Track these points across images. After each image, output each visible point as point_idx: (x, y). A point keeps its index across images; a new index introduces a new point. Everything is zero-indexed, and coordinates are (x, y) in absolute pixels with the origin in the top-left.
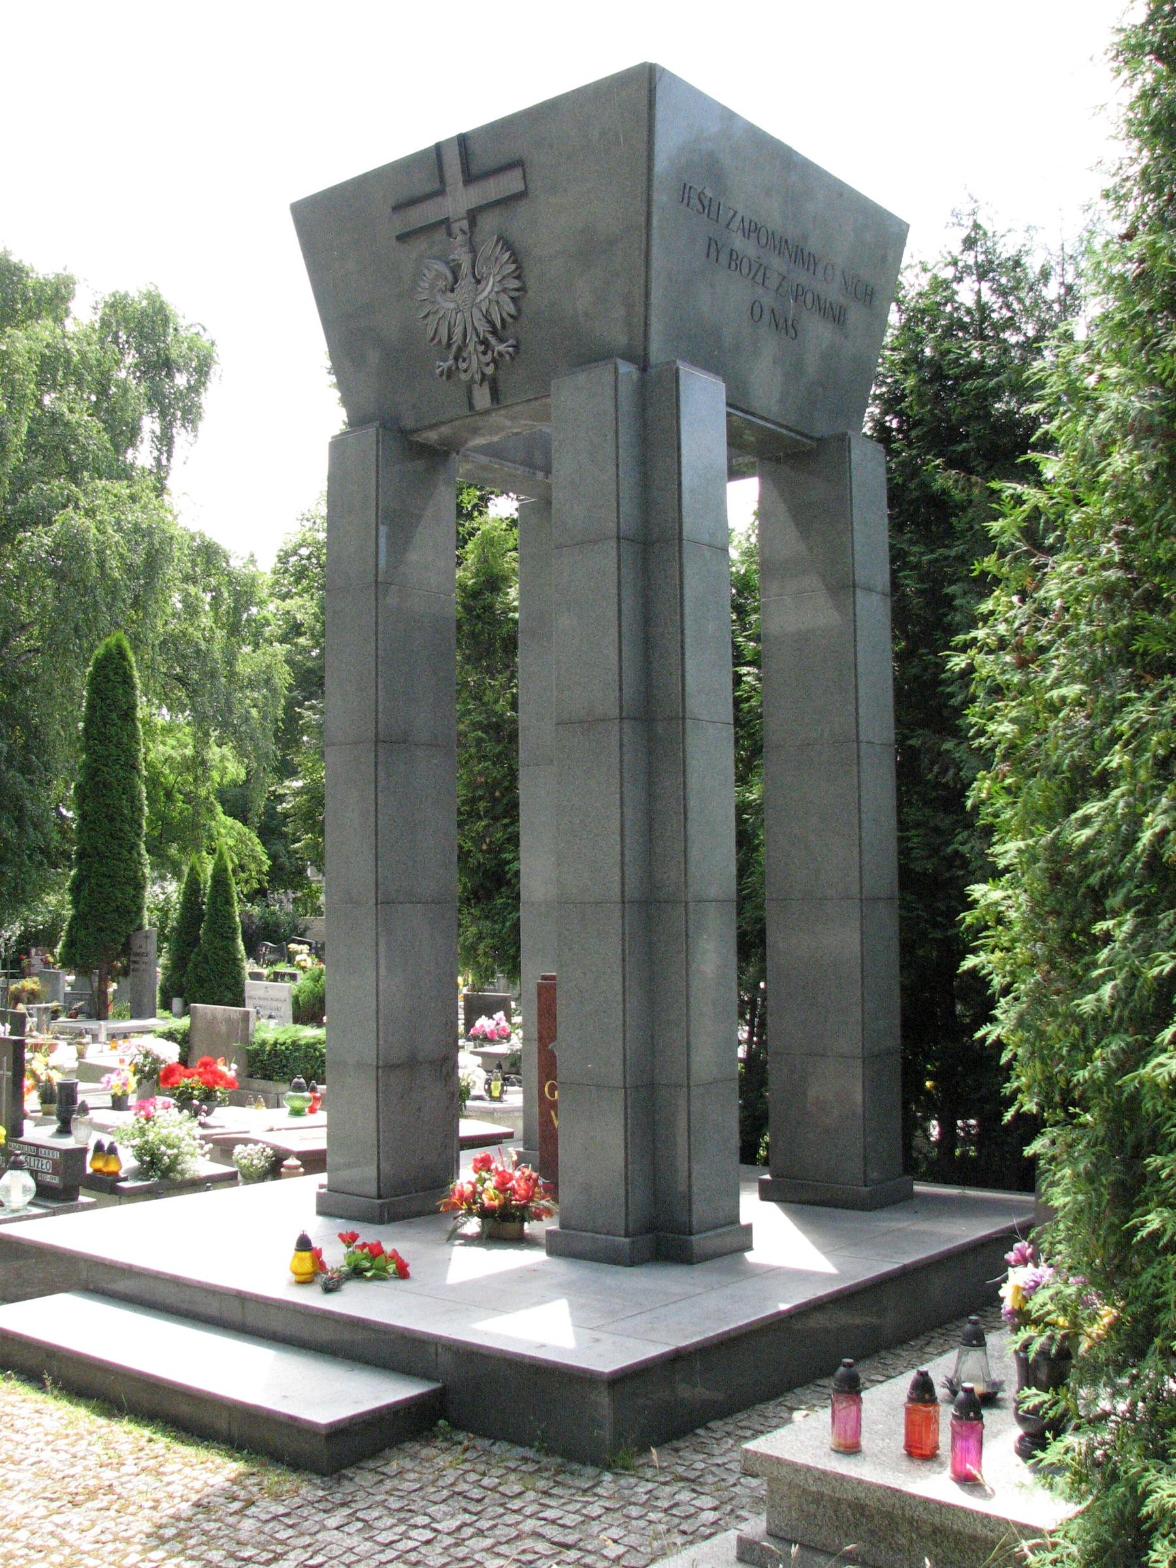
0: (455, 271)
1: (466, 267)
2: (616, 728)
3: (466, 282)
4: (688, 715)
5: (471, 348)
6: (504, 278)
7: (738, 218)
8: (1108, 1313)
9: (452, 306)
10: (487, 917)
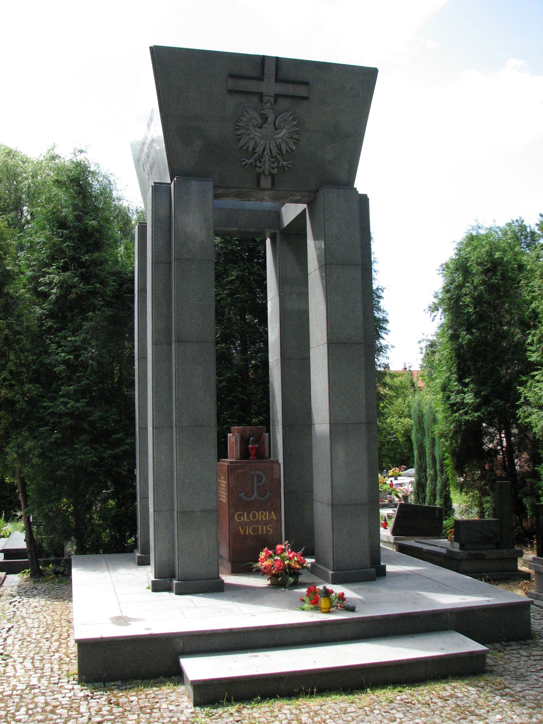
0: (265, 119)
8: (110, 501)
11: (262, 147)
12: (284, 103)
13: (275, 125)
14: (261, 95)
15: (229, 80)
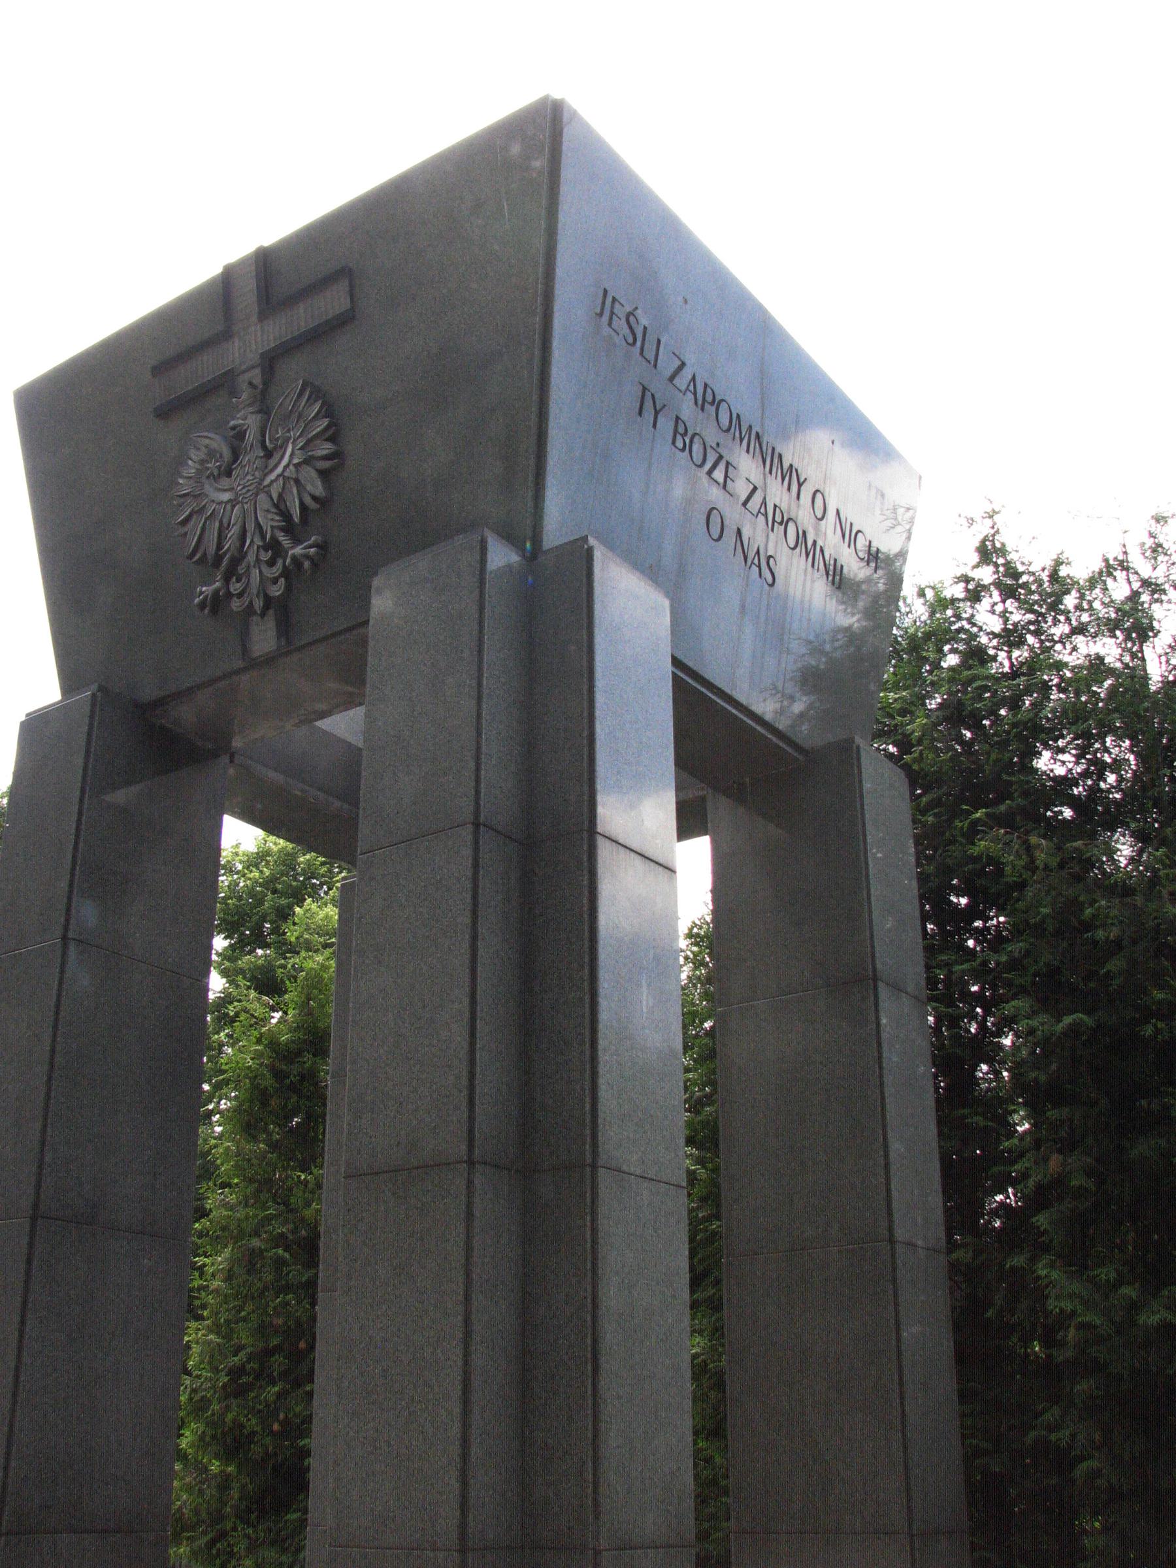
1: (251, 436)
2: (461, 1182)
3: (251, 458)
4: (603, 1159)
5: (251, 558)
6: (309, 442)
7: (687, 374)
9: (226, 496)
10: (273, 1543)
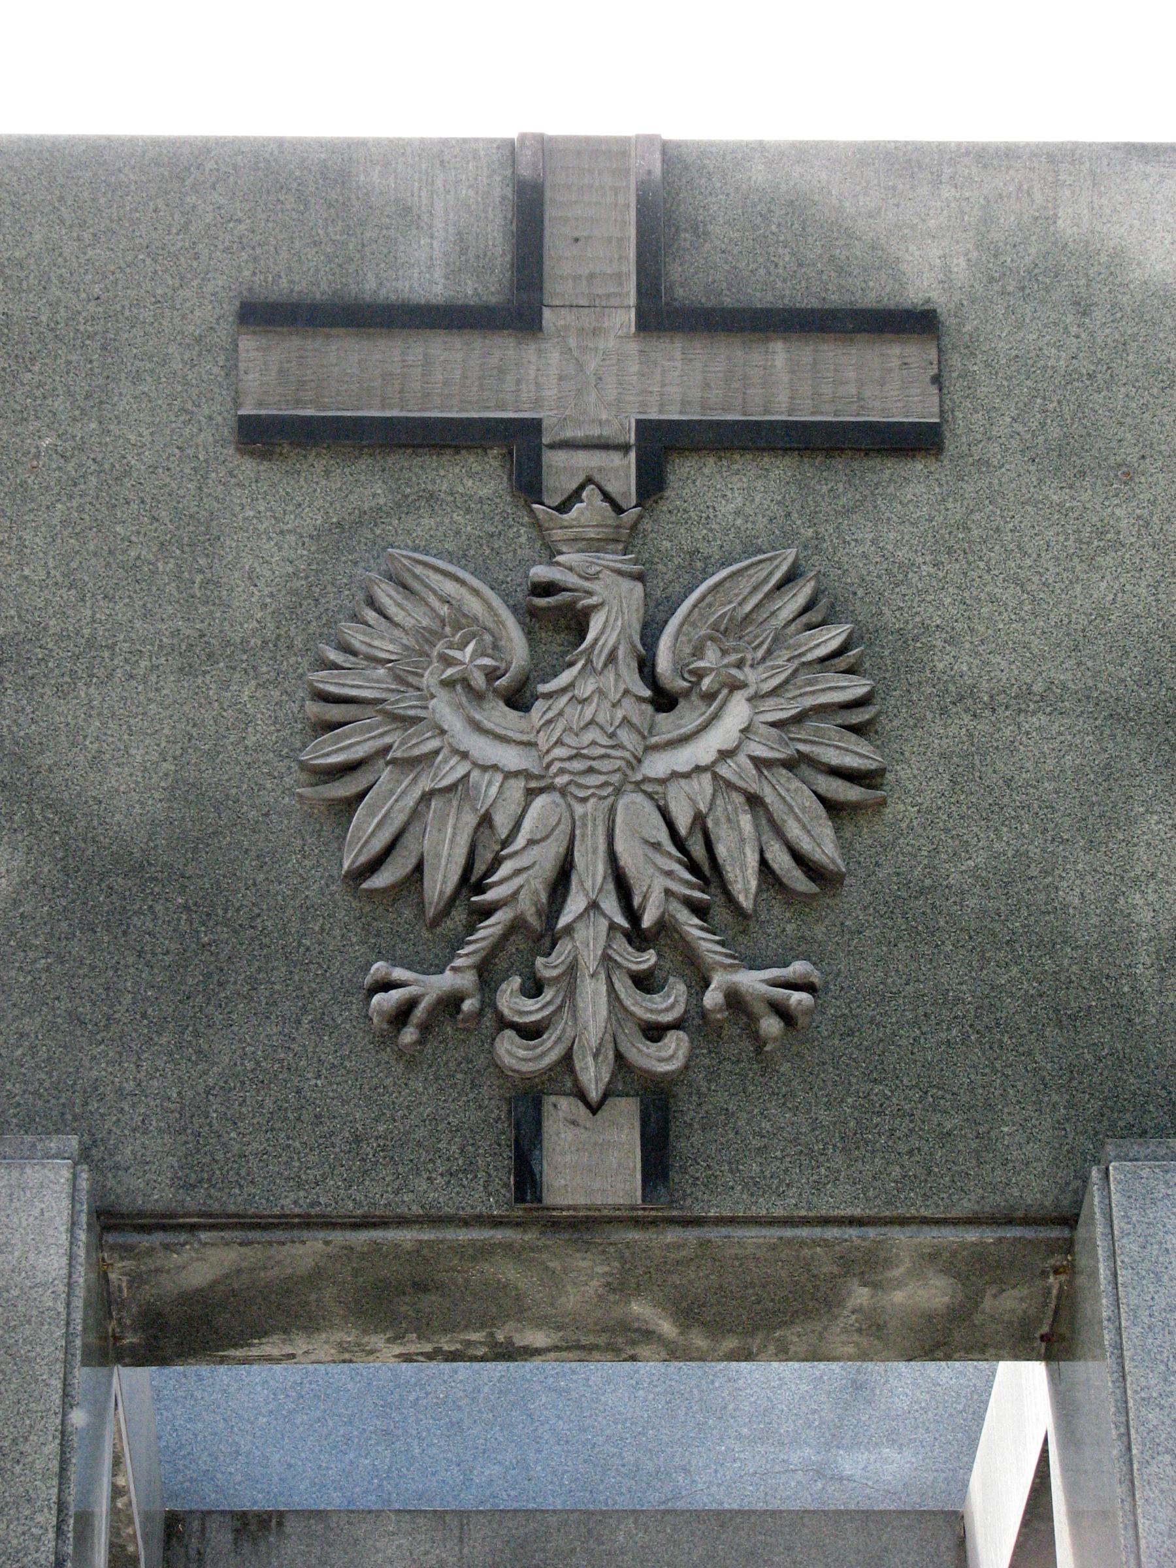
0: (558, 620)
11: (546, 857)
12: (725, 497)
13: (646, 667)
14: (519, 447)
15: (248, 344)
